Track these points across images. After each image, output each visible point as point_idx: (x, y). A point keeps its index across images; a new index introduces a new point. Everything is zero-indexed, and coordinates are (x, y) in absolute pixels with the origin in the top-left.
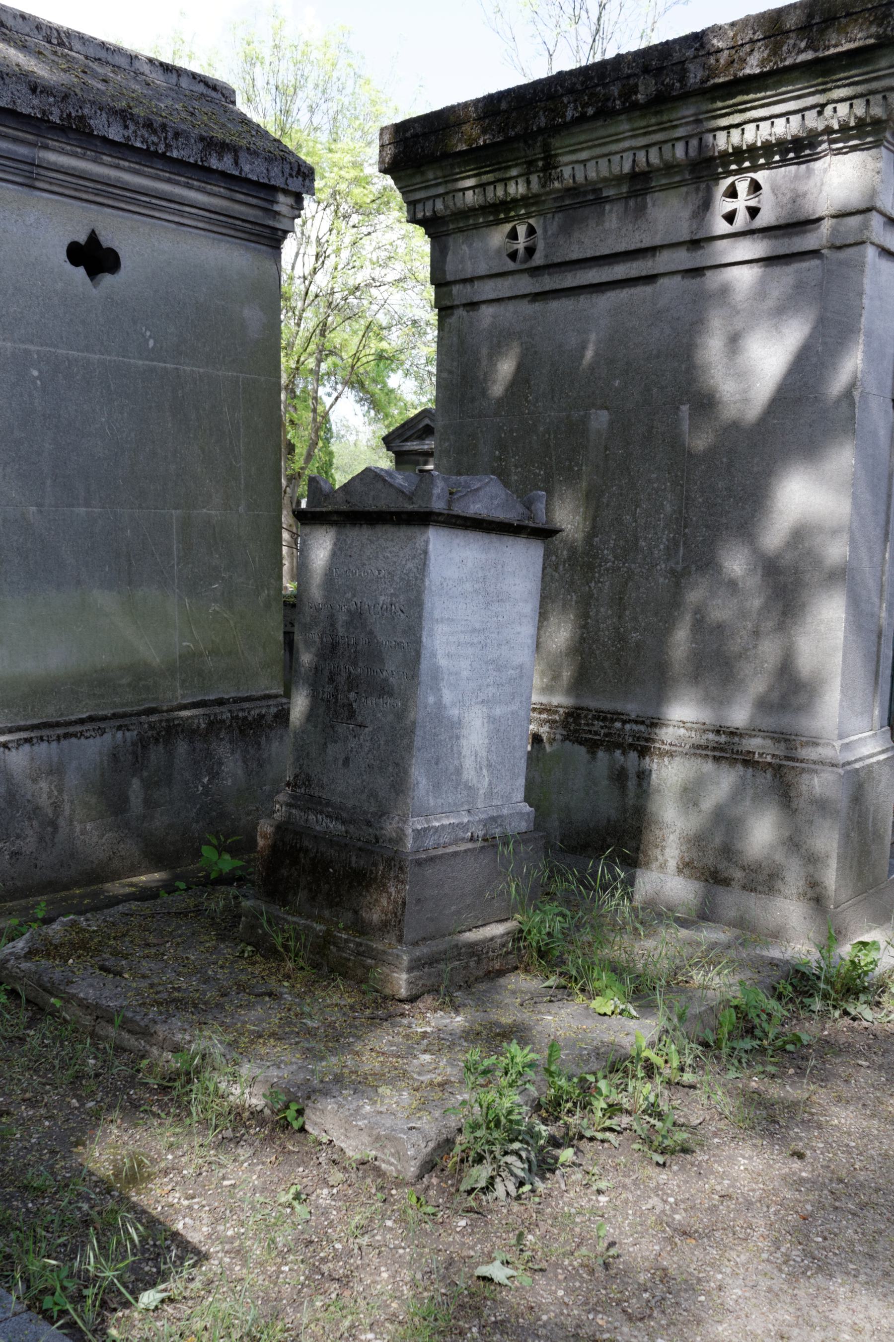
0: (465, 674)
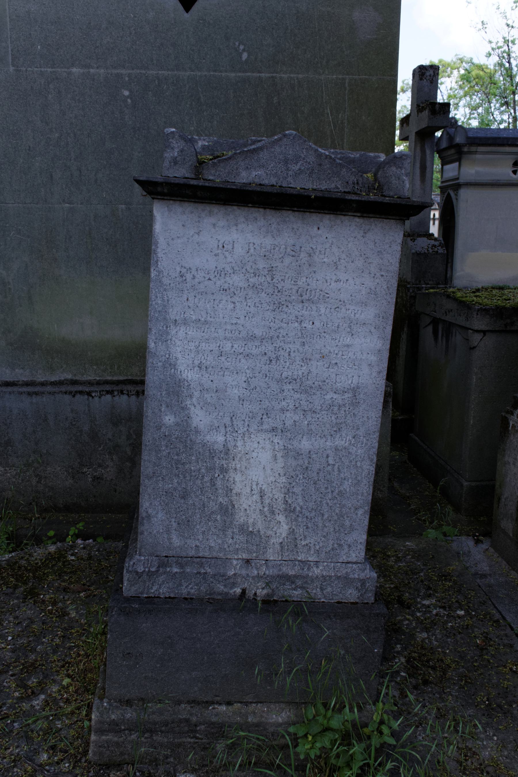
0: (235, 392)
